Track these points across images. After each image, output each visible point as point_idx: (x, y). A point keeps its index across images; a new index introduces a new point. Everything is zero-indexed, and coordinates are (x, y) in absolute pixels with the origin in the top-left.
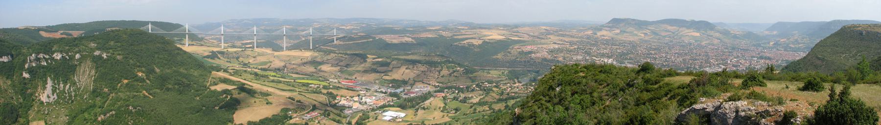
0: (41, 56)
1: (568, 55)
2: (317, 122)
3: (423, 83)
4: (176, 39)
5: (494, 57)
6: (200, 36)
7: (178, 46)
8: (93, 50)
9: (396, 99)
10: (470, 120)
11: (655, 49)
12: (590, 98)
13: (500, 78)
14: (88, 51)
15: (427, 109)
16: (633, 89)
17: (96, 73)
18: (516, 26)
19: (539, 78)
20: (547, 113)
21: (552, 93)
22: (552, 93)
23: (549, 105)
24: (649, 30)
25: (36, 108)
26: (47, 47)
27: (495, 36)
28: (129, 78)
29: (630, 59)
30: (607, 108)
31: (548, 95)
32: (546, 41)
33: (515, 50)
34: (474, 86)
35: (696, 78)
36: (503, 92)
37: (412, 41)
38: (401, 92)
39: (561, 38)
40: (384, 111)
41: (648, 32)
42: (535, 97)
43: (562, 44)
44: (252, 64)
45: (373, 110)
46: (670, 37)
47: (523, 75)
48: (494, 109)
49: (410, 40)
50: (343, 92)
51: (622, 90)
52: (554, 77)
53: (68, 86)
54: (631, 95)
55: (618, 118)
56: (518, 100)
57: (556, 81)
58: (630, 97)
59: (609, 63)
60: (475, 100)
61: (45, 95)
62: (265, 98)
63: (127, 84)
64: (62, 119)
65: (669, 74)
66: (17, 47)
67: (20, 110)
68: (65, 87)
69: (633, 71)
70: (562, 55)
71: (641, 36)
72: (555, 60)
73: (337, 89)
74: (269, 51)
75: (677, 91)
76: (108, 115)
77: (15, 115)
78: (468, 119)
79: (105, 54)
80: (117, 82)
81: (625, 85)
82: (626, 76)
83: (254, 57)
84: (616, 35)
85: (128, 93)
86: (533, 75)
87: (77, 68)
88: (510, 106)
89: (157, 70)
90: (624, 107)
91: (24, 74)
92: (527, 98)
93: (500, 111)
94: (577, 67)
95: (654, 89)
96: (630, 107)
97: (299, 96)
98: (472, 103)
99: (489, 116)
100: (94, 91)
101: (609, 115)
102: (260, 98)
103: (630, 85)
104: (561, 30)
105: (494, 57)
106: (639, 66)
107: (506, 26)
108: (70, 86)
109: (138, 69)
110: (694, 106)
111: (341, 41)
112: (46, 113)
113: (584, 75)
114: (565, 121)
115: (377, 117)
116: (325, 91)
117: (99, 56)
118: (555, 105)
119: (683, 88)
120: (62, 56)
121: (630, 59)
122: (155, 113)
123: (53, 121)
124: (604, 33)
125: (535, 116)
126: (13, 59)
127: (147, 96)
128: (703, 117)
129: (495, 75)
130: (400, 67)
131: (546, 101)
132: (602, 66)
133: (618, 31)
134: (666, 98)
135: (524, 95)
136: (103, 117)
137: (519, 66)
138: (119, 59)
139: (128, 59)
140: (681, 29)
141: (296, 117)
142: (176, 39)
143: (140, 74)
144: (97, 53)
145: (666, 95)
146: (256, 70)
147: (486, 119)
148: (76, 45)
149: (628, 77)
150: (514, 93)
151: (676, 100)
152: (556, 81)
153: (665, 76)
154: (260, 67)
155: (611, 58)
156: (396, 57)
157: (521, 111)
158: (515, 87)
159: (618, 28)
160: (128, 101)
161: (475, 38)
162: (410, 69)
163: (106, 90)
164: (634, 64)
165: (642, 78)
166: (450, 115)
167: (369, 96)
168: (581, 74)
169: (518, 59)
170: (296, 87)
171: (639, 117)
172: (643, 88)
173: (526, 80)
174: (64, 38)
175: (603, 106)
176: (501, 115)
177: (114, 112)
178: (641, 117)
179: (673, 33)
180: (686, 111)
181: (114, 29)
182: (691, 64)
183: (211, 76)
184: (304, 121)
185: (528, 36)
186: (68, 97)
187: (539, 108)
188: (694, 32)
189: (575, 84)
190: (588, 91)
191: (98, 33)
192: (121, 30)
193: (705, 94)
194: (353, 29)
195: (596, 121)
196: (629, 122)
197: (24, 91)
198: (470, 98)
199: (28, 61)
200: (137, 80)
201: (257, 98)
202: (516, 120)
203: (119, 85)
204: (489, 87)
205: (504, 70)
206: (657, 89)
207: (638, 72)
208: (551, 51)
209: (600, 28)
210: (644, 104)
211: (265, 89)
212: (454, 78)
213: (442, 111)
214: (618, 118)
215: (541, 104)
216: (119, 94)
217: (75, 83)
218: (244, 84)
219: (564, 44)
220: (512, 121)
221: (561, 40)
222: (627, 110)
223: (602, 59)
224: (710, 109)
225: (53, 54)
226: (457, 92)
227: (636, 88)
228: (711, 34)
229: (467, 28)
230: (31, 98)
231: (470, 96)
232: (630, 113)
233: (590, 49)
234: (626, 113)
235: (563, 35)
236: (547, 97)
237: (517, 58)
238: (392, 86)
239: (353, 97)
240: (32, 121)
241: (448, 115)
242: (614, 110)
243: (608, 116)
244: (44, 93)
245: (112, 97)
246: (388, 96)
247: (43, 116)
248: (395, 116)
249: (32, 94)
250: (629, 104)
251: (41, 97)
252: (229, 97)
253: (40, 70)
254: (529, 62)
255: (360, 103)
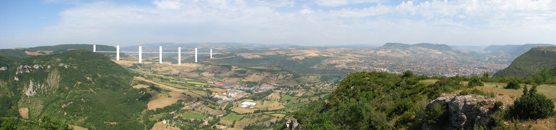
0: (26, 66)
1: (359, 66)
2: (200, 108)
3: (267, 84)
4: (111, 56)
5: (312, 67)
6: (126, 54)
7: (112, 60)
8: (59, 63)
9: (250, 94)
10: (297, 107)
11: (413, 62)
12: (372, 94)
13: (316, 80)
14: (55, 63)
15: (270, 100)
16: (399, 87)
17: (61, 77)
18: (326, 48)
19: (340, 80)
20: (345, 103)
21: (348, 90)
22: (348, 90)
23: (346, 98)
24: (410, 50)
25: (23, 100)
26: (30, 61)
27: (313, 54)
28: (81, 81)
29: (398, 68)
30: (383, 100)
31: (346, 91)
32: (345, 57)
33: (325, 63)
34: (299, 86)
35: (439, 80)
36: (317, 90)
37: (260, 57)
38: (253, 89)
39: (354, 55)
40: (242, 102)
41: (409, 51)
42: (337, 92)
43: (355, 59)
44: (159, 72)
45: (235, 101)
46: (422, 55)
47: (330, 79)
48: (312, 101)
49: (259, 56)
50: (217, 89)
51: (393, 88)
52: (349, 80)
53: (43, 86)
54: (398, 91)
55: (390, 106)
56: (327, 94)
57: (351, 83)
58: (398, 92)
59: (384, 71)
60: (300, 95)
61: (28, 91)
62: (167, 93)
63: (80, 85)
64: (39, 107)
65: (423, 78)
66: (10, 60)
67: (13, 101)
68: (41, 86)
69: (399, 76)
70: (355, 66)
71: (404, 54)
72: (350, 69)
73: (213, 88)
74: (169, 63)
75: (427, 89)
76: (68, 104)
77: (9, 104)
78: (295, 107)
79: (66, 66)
80: (74, 83)
81: (394, 85)
82: (395, 80)
83: (160, 67)
84: (389, 53)
85: (81, 90)
86: (336, 79)
87: (49, 75)
88: (322, 98)
89: (99, 76)
90: (394, 99)
91: (15, 78)
92: (333, 93)
93: (315, 101)
94: (364, 74)
95: (413, 88)
96: (397, 99)
97: (189, 92)
98: (298, 96)
99: (309, 105)
100: (59, 89)
101: (384, 104)
102: (164, 93)
103: (398, 85)
104: (354, 50)
105: (312, 67)
106: (403, 73)
107: (319, 48)
108: (44, 86)
109: (87, 75)
110: (438, 99)
111: (215, 57)
112: (29, 102)
113: (368, 79)
114: (357, 108)
115: (238, 105)
116: (205, 89)
117: (62, 66)
118: (350, 97)
119: (431, 87)
120: (39, 67)
121: (398, 68)
122: (98, 103)
123: (33, 108)
124: (381, 52)
125: (337, 105)
126: (8, 69)
127: (93, 92)
128: (444, 105)
129: (312, 78)
130: (253, 74)
131: (344, 95)
132: (380, 73)
133: (390, 51)
134: (421, 93)
135: (331, 91)
136: (65, 105)
137: (327, 73)
138: (75, 68)
139: (81, 69)
140: (430, 50)
141: (187, 106)
142: (111, 56)
143: (88, 78)
144: (61, 65)
145: (420, 91)
146: (162, 76)
147: (307, 107)
148: (48, 60)
149: (396, 80)
150: (324, 90)
151: (427, 94)
152: (351, 83)
153: (419, 79)
154: (164, 74)
155: (386, 68)
156: (250, 67)
157: (329, 102)
158: (325, 86)
159: (390, 49)
160: (80, 95)
161: (300, 56)
162: (258, 75)
163: (67, 88)
164: (400, 72)
165: (405, 81)
166: (284, 104)
167: (233, 92)
168: (367, 78)
169: (327, 69)
170: (187, 87)
171: (403, 106)
172: (406, 87)
173: (332, 82)
174: (41, 55)
175: (381, 99)
176: (316, 104)
177: (72, 102)
178: (404, 105)
179: (425, 52)
180: (433, 101)
181: (72, 49)
182: (436, 72)
183: (133, 80)
184: (192, 108)
185: (333, 54)
186: (43, 93)
187: (340, 100)
188: (438, 51)
189: (363, 85)
190: (371, 89)
191: (62, 52)
192: (77, 51)
193: (445, 91)
194: (223, 50)
195: (376, 108)
196: (397, 108)
197: (15, 89)
198: (297, 94)
199: (18, 70)
200: (87, 82)
201: (162, 93)
202: (325, 107)
203: (75, 85)
204: (309, 86)
205: (318, 75)
206: (415, 88)
207: (403, 77)
208: (348, 64)
209: (379, 49)
210: (406, 97)
211: (167, 87)
212: (287, 81)
213: (279, 102)
214: (390, 106)
215: (342, 97)
216: (75, 91)
217: (47, 84)
218: (154, 85)
219: (357, 59)
220: (323, 108)
221: (354, 57)
222: (396, 101)
223: (380, 69)
224: (448, 100)
225: (33, 66)
226: (288, 89)
227: (402, 87)
228: (449, 53)
229: (295, 49)
230: (20, 94)
231: (297, 92)
232: (397, 103)
233: (373, 62)
234: (395, 103)
235: (355, 54)
236: (345, 93)
237: (327, 68)
238: (248, 85)
239: (223, 92)
240: (20, 108)
241: (283, 104)
242: (387, 101)
243: (384, 105)
244: (28, 90)
245: (71, 93)
246: (245, 92)
247: (27, 105)
248: (249, 105)
249: (20, 91)
250: (397, 97)
251: (26, 92)
252: (145, 93)
253: (25, 76)
254: (334, 71)
255: (227, 97)
